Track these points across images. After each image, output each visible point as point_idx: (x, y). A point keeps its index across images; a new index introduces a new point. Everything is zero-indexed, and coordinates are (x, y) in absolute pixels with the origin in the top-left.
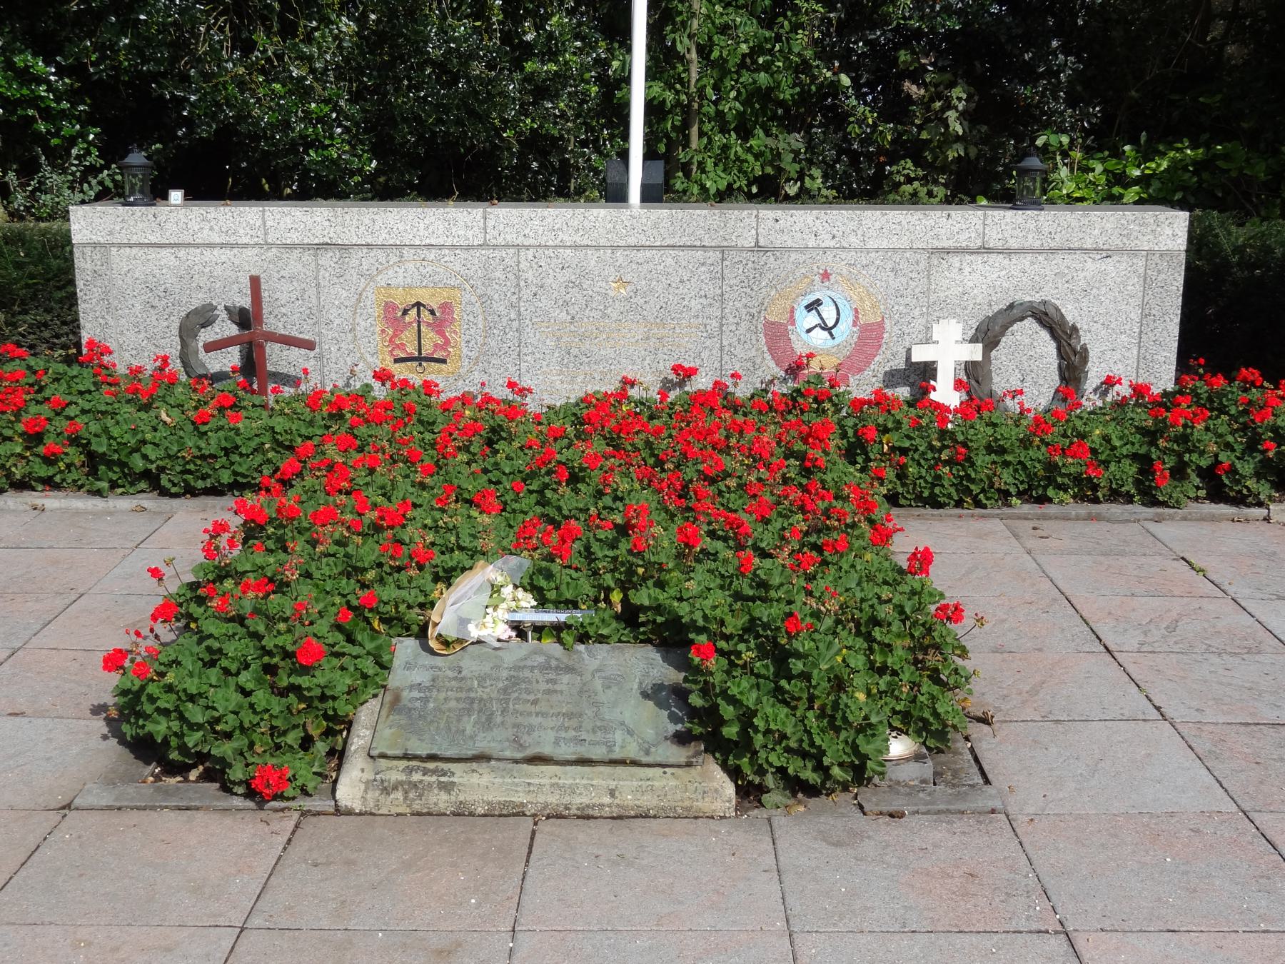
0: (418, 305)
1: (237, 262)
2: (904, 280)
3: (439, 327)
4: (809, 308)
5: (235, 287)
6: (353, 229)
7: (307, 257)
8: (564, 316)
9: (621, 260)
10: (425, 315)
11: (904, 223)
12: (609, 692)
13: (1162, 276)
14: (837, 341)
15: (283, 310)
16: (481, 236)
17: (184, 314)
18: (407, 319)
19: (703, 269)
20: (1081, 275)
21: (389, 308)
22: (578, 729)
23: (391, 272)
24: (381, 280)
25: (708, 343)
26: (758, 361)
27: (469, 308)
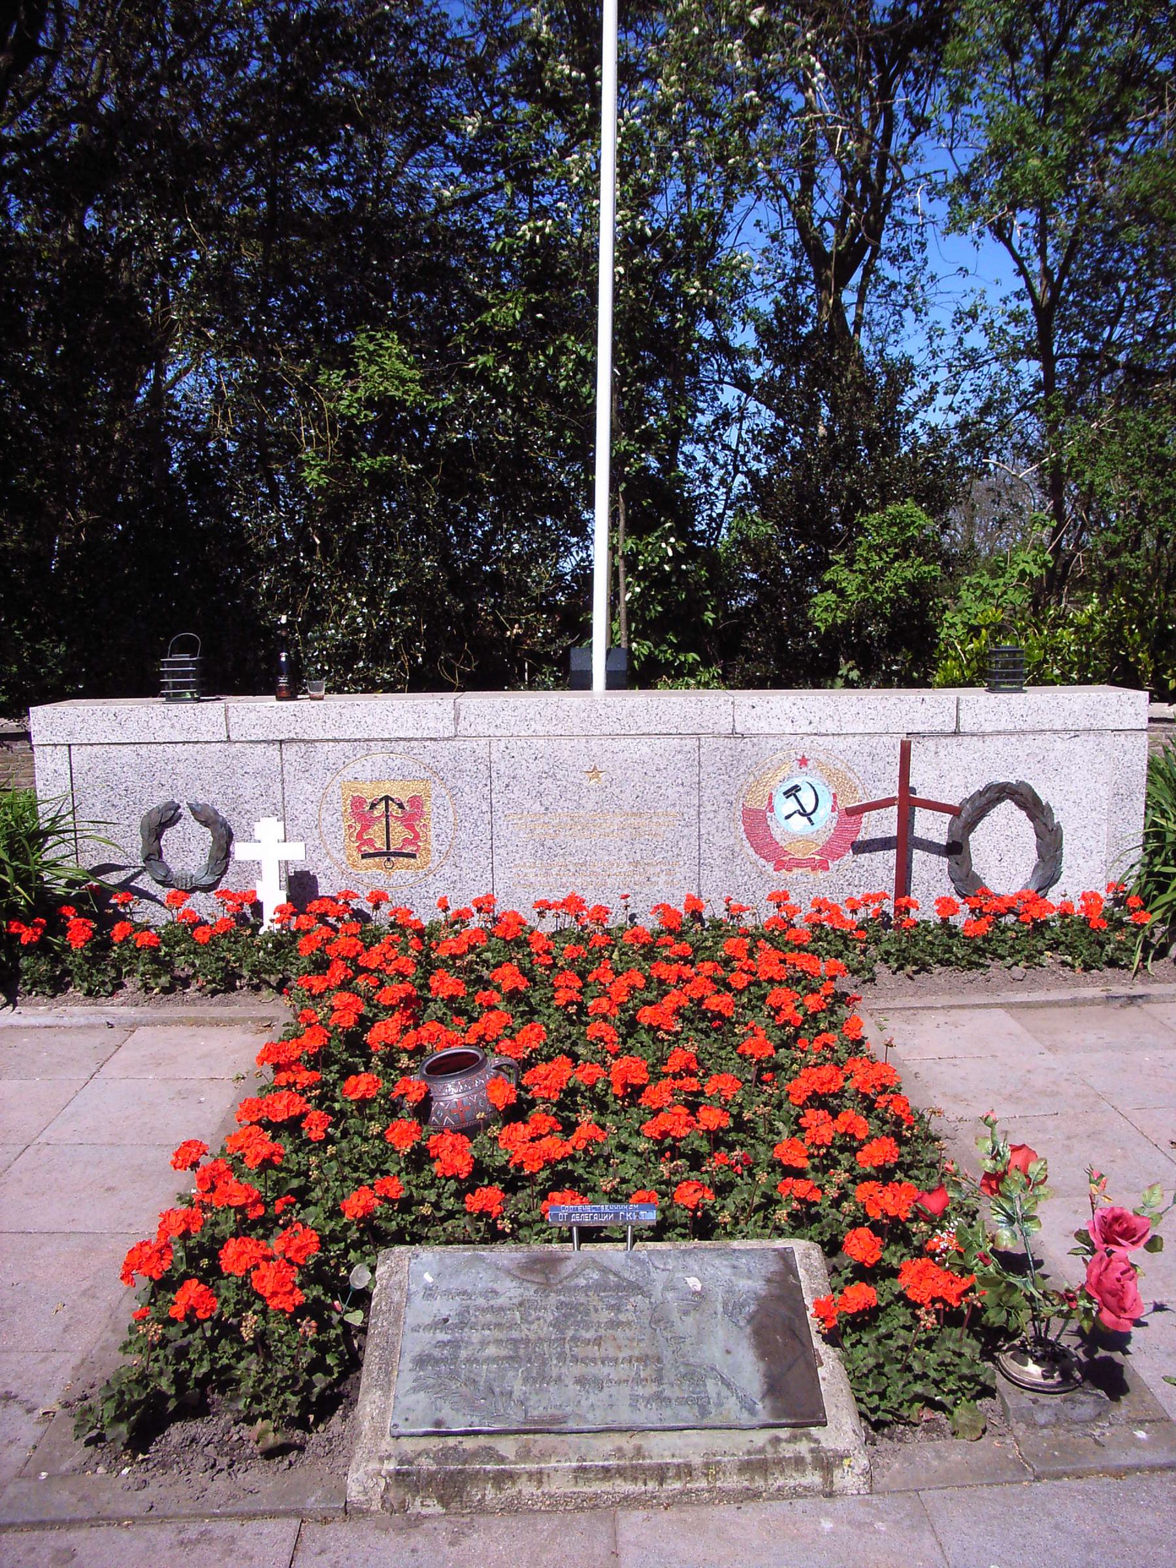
0: (387, 799)
1: (200, 758)
2: (881, 765)
3: (409, 822)
4: (787, 794)
5: (198, 783)
6: (319, 723)
7: (273, 751)
8: (537, 807)
9: (595, 749)
10: (393, 807)
11: (880, 708)
12: (689, 1320)
13: (1128, 756)
14: (816, 827)
15: (247, 807)
16: (452, 729)
17: (144, 813)
18: (376, 813)
19: (679, 757)
20: (1052, 755)
21: (358, 802)
22: (659, 1380)
23: (358, 767)
24: (348, 773)
25: (686, 831)
26: (737, 849)
27: (439, 801)
